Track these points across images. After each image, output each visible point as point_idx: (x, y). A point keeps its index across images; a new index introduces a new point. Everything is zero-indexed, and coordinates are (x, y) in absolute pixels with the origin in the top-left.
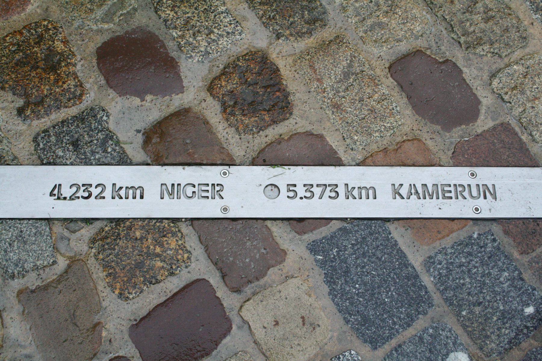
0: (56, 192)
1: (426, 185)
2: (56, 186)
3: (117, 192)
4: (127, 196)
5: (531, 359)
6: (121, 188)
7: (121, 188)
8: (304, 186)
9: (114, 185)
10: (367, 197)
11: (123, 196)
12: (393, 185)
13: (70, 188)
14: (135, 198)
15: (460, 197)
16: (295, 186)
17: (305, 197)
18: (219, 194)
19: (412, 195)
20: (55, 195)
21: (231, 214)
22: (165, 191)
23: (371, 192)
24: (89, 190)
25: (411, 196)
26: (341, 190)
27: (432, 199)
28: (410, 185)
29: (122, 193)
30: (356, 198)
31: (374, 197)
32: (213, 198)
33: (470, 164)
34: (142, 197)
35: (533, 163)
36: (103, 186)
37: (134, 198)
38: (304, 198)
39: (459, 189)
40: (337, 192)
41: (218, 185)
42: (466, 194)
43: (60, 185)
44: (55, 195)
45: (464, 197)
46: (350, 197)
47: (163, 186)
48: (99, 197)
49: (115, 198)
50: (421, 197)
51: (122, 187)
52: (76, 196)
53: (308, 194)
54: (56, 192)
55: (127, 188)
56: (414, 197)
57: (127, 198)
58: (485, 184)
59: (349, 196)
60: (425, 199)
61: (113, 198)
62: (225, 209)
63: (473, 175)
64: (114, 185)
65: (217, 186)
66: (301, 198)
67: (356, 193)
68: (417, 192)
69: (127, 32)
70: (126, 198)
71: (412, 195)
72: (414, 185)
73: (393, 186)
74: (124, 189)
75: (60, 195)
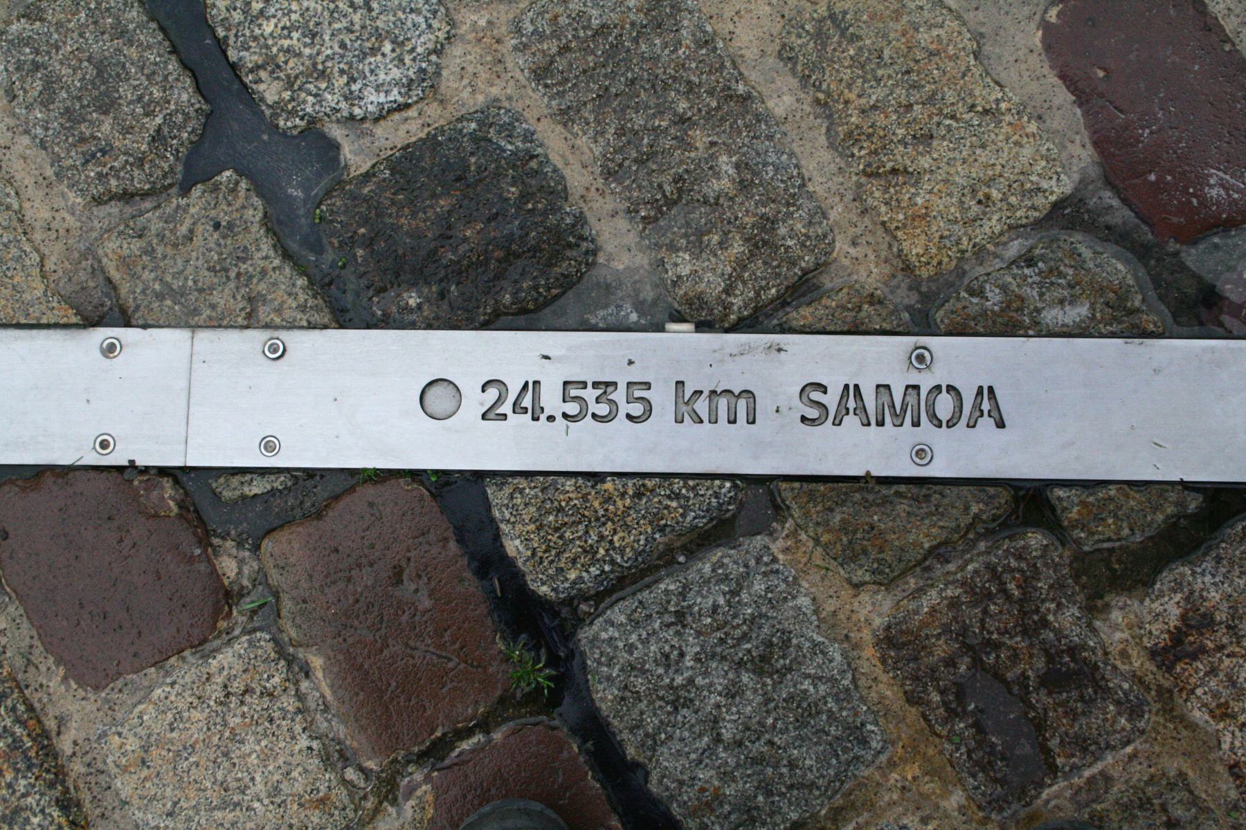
0: (527, 402)
1: (888, 387)
2: (526, 384)
3: (687, 403)
5: (307, 828)
6: (698, 393)
10: (503, 417)
11: (705, 417)
13: (483, 391)
16: (648, 386)
17: (565, 416)
20: (525, 410)
21: (936, 470)
23: (742, 404)
24: (609, 397)
25: (845, 417)
26: (662, 397)
27: (901, 425)
28: (846, 387)
29: (702, 406)
30: (701, 422)
32: (713, 420)
33: (1228, 335)
36: (497, 385)
37: (732, 421)
40: (611, 402)
43: (536, 383)
44: (525, 410)
47: (569, 387)
48: (491, 415)
49: (682, 422)
51: (701, 392)
52: (498, 412)
54: (527, 402)
55: (713, 392)
56: (851, 421)
58: (824, 383)
62: (269, 446)
63: (275, 351)
64: (680, 384)
66: (551, 418)
67: (702, 406)
68: (862, 409)
75: (538, 410)
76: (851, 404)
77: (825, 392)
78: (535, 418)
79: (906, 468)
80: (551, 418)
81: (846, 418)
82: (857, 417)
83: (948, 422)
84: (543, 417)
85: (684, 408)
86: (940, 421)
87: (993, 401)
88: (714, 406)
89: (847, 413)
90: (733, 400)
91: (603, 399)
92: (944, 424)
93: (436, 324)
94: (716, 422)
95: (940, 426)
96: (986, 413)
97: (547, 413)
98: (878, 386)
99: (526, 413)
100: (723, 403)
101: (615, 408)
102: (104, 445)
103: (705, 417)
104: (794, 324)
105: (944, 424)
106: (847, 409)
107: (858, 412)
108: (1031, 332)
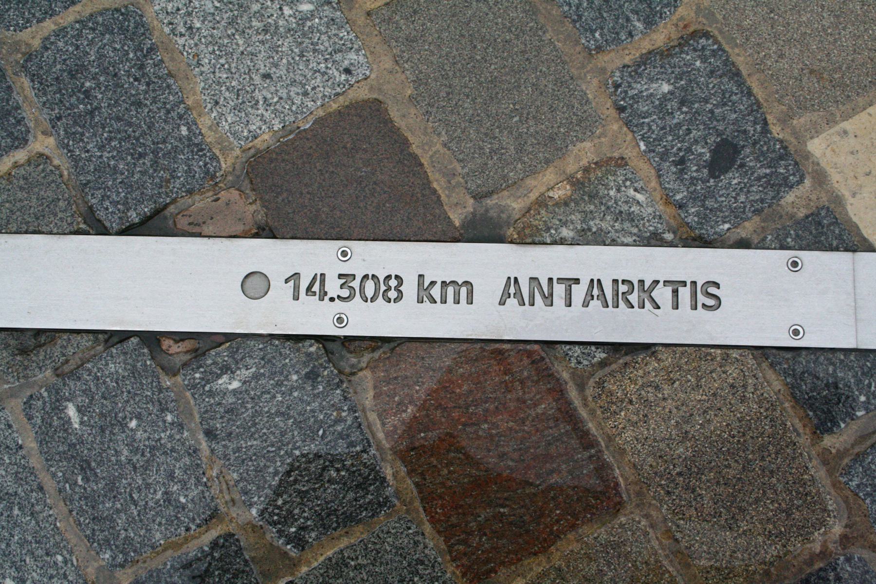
0: (316, 288)
1: (536, 279)
2: (314, 278)
4: (444, 299)
6: (433, 283)
7: (433, 283)
8: (339, 278)
9: (421, 276)
10: (641, 305)
11: (438, 299)
12: (421, 276)
14: (445, 302)
15: (621, 303)
17: (339, 297)
18: (626, 298)
19: (593, 299)
20: (314, 293)
22: (536, 290)
23: (464, 290)
25: (591, 302)
28: (592, 281)
29: (436, 292)
31: (568, 302)
32: (457, 301)
34: (470, 302)
35: (864, 246)
38: (337, 300)
39: (623, 288)
41: (624, 281)
42: (634, 298)
43: (323, 275)
44: (314, 293)
45: (630, 303)
46: (425, 299)
50: (610, 303)
53: (345, 293)
54: (316, 288)
55: (443, 282)
57: (444, 301)
59: (646, 300)
60: (617, 307)
61: (420, 301)
65: (623, 283)
66: (332, 299)
67: (436, 292)
68: (519, 294)
69: (831, 121)
70: (530, 305)
71: (593, 299)
72: (599, 281)
73: (625, 283)
74: (438, 285)
76: (512, 290)
77: (719, 288)
78: (321, 299)
79: (329, 329)
80: (332, 299)
81: (591, 302)
82: (600, 302)
83: (371, 298)
84: (327, 298)
85: (422, 293)
86: (390, 299)
87: (517, 286)
88: (444, 291)
89: (509, 297)
90: (457, 288)
91: (346, 286)
92: (392, 301)
93: (653, 242)
94: (472, 303)
95: (390, 302)
96: (512, 295)
97: (329, 295)
98: (531, 278)
99: (315, 295)
100: (450, 290)
101: (400, 295)
102: (340, 320)
103: (438, 299)
104: (44, 230)
105: (392, 301)
106: (509, 294)
107: (600, 297)
108: (566, 233)
